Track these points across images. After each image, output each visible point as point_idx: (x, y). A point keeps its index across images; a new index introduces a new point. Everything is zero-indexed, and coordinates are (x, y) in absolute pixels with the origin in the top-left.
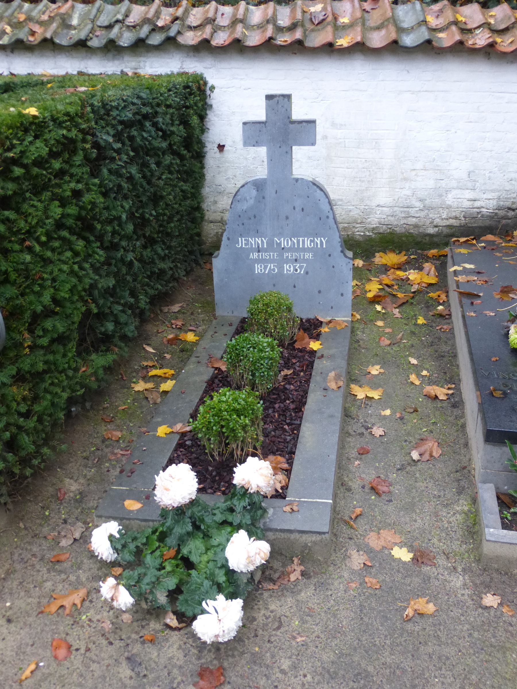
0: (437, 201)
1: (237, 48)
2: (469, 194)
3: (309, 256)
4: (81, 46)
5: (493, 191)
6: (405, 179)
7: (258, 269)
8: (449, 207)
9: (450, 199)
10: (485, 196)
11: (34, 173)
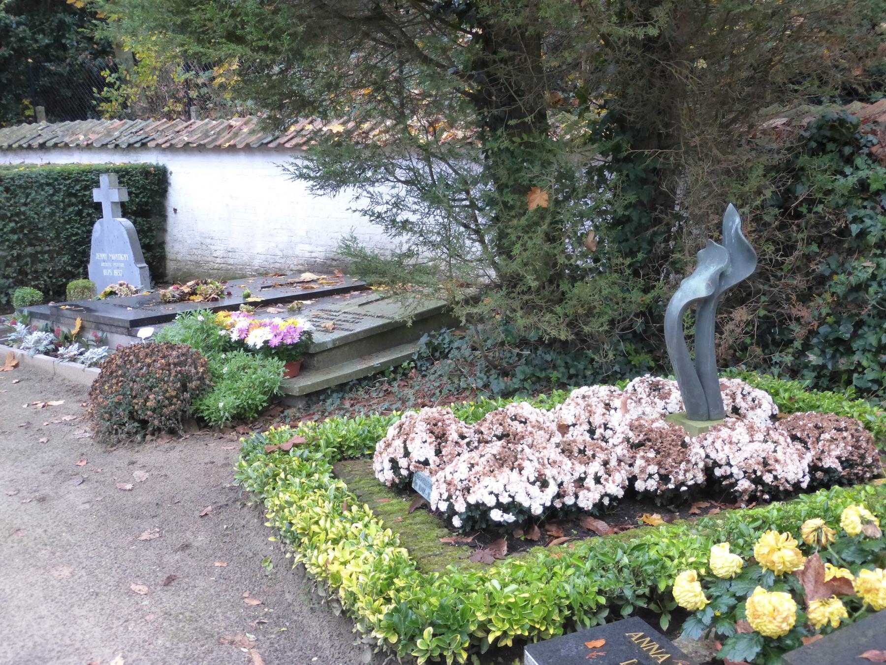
0: (290, 252)
1: (187, 148)
2: (308, 248)
3: (122, 265)
4: (89, 147)
5: (322, 246)
6: (271, 235)
7: (105, 272)
8: (297, 257)
9: (297, 252)
10: (318, 249)
11: (799, 277)
